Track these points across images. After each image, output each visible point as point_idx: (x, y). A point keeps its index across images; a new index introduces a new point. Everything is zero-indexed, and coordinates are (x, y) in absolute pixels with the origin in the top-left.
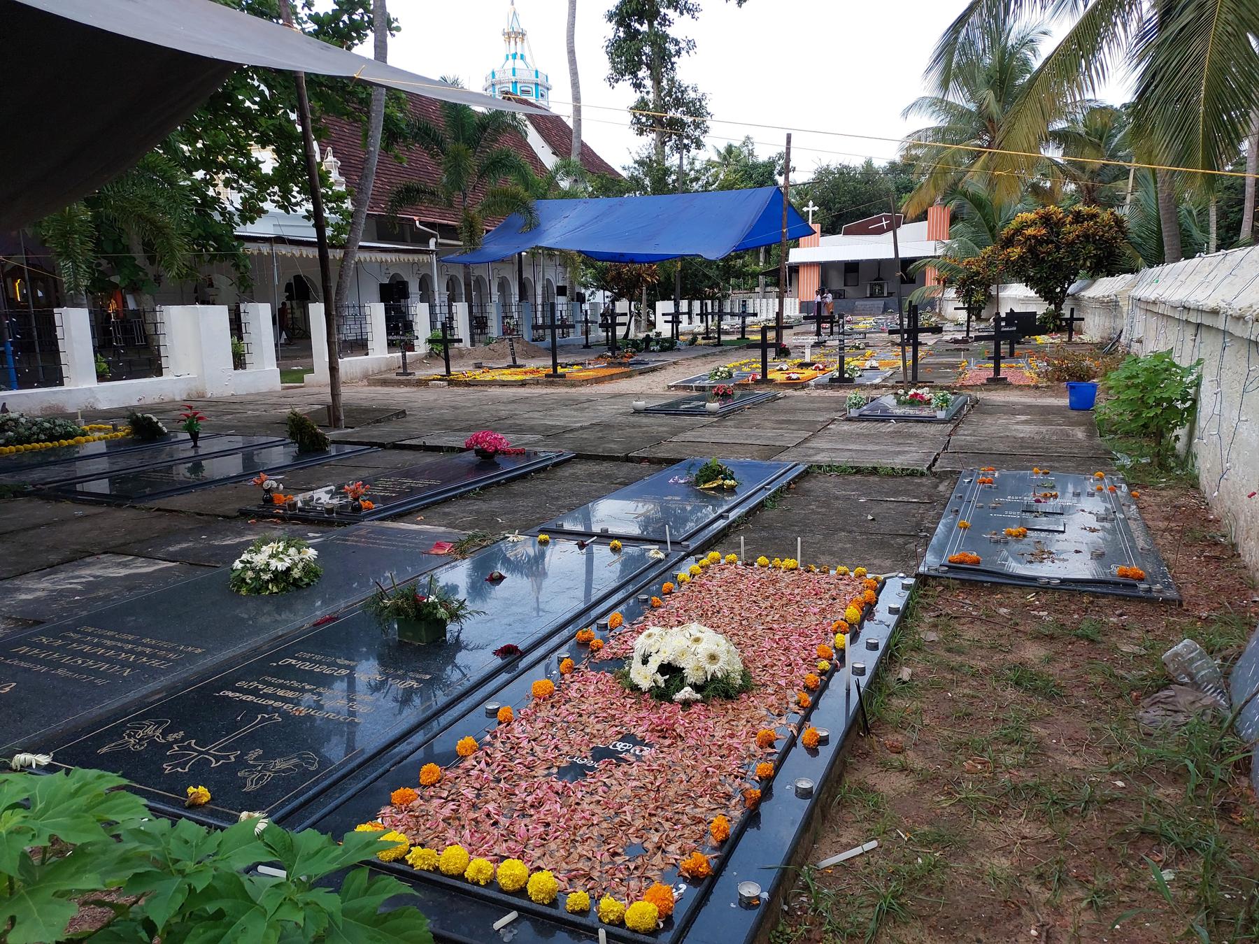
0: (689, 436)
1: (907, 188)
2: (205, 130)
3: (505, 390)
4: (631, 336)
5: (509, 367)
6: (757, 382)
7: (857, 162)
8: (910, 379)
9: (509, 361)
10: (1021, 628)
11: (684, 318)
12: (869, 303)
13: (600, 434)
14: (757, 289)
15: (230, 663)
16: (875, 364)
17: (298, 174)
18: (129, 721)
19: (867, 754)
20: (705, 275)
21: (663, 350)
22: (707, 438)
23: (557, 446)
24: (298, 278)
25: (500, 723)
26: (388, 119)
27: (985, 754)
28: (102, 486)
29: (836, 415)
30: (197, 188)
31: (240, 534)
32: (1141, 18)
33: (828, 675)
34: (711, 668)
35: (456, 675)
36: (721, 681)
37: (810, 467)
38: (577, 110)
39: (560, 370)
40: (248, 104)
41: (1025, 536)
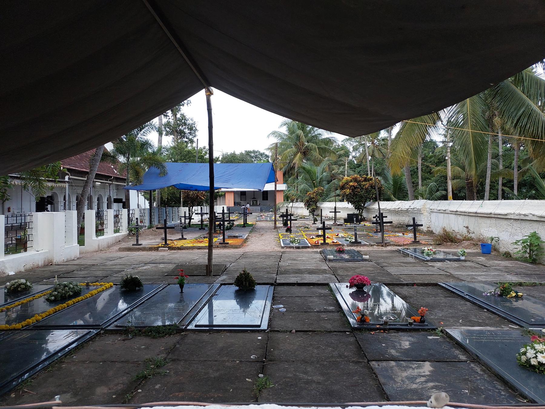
5: (180, 239)
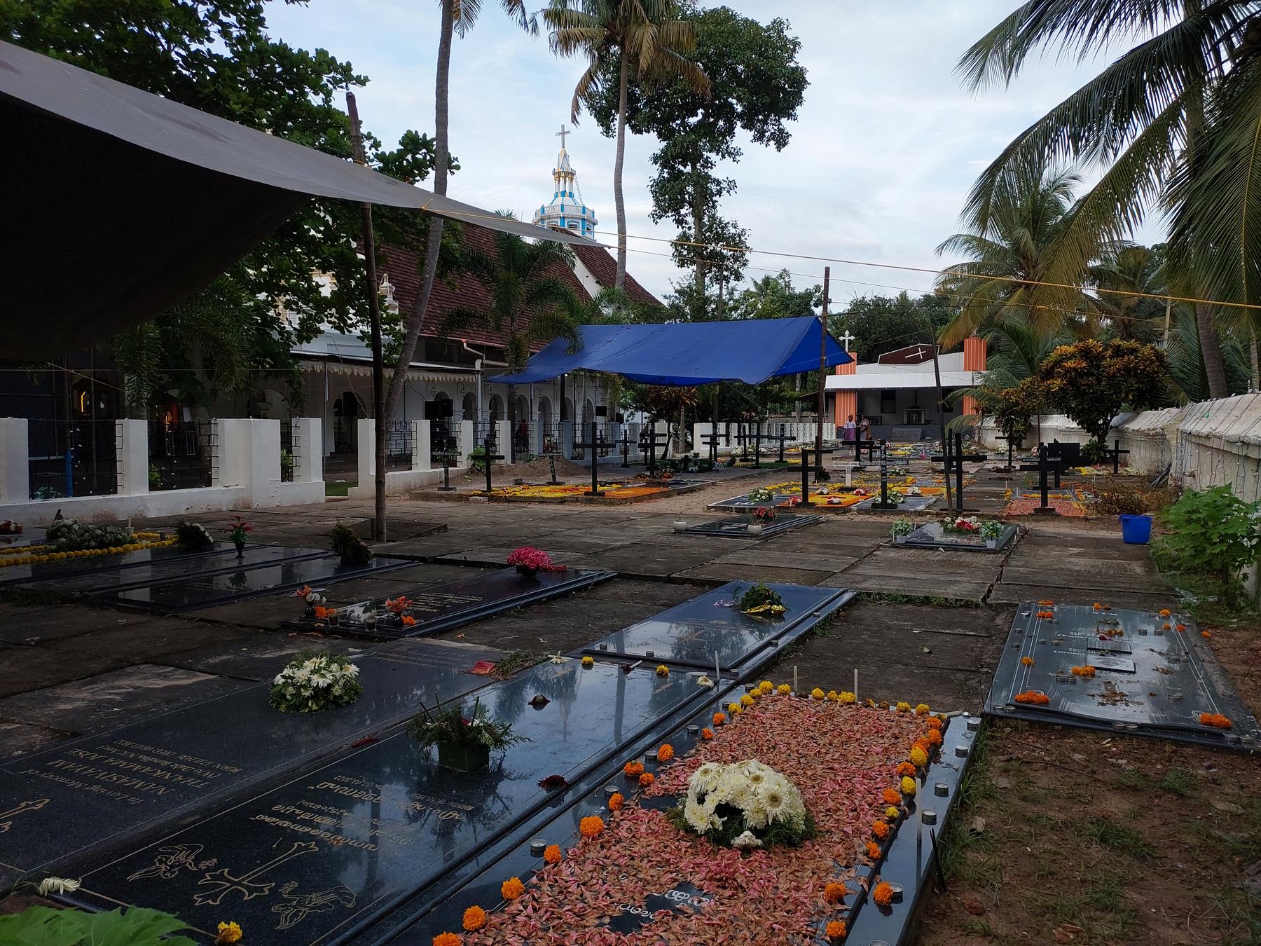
0: (731, 558)
1: (943, 320)
2: (271, 255)
3: (544, 505)
4: (669, 456)
5: (549, 484)
6: (798, 505)
7: (892, 294)
8: (955, 506)
9: (549, 478)
10: (1100, 777)
11: (722, 440)
12: (906, 430)
13: (641, 554)
14: (793, 414)
15: (268, 783)
16: (917, 490)
17: (356, 295)
18: (162, 845)
19: (945, 915)
20: (742, 399)
21: (702, 470)
22: (751, 560)
23: (598, 565)
24: (349, 396)
25: (547, 863)
26: (444, 248)
27: (1077, 921)
28: (143, 595)
29: (882, 542)
30: (260, 308)
31: (280, 647)
32: (1174, 165)
33: (896, 822)
34: (773, 811)
35: (498, 806)
36: (783, 826)
37: (859, 594)
38: (622, 241)
39: (599, 488)
40: (312, 232)
41: (1093, 676)
